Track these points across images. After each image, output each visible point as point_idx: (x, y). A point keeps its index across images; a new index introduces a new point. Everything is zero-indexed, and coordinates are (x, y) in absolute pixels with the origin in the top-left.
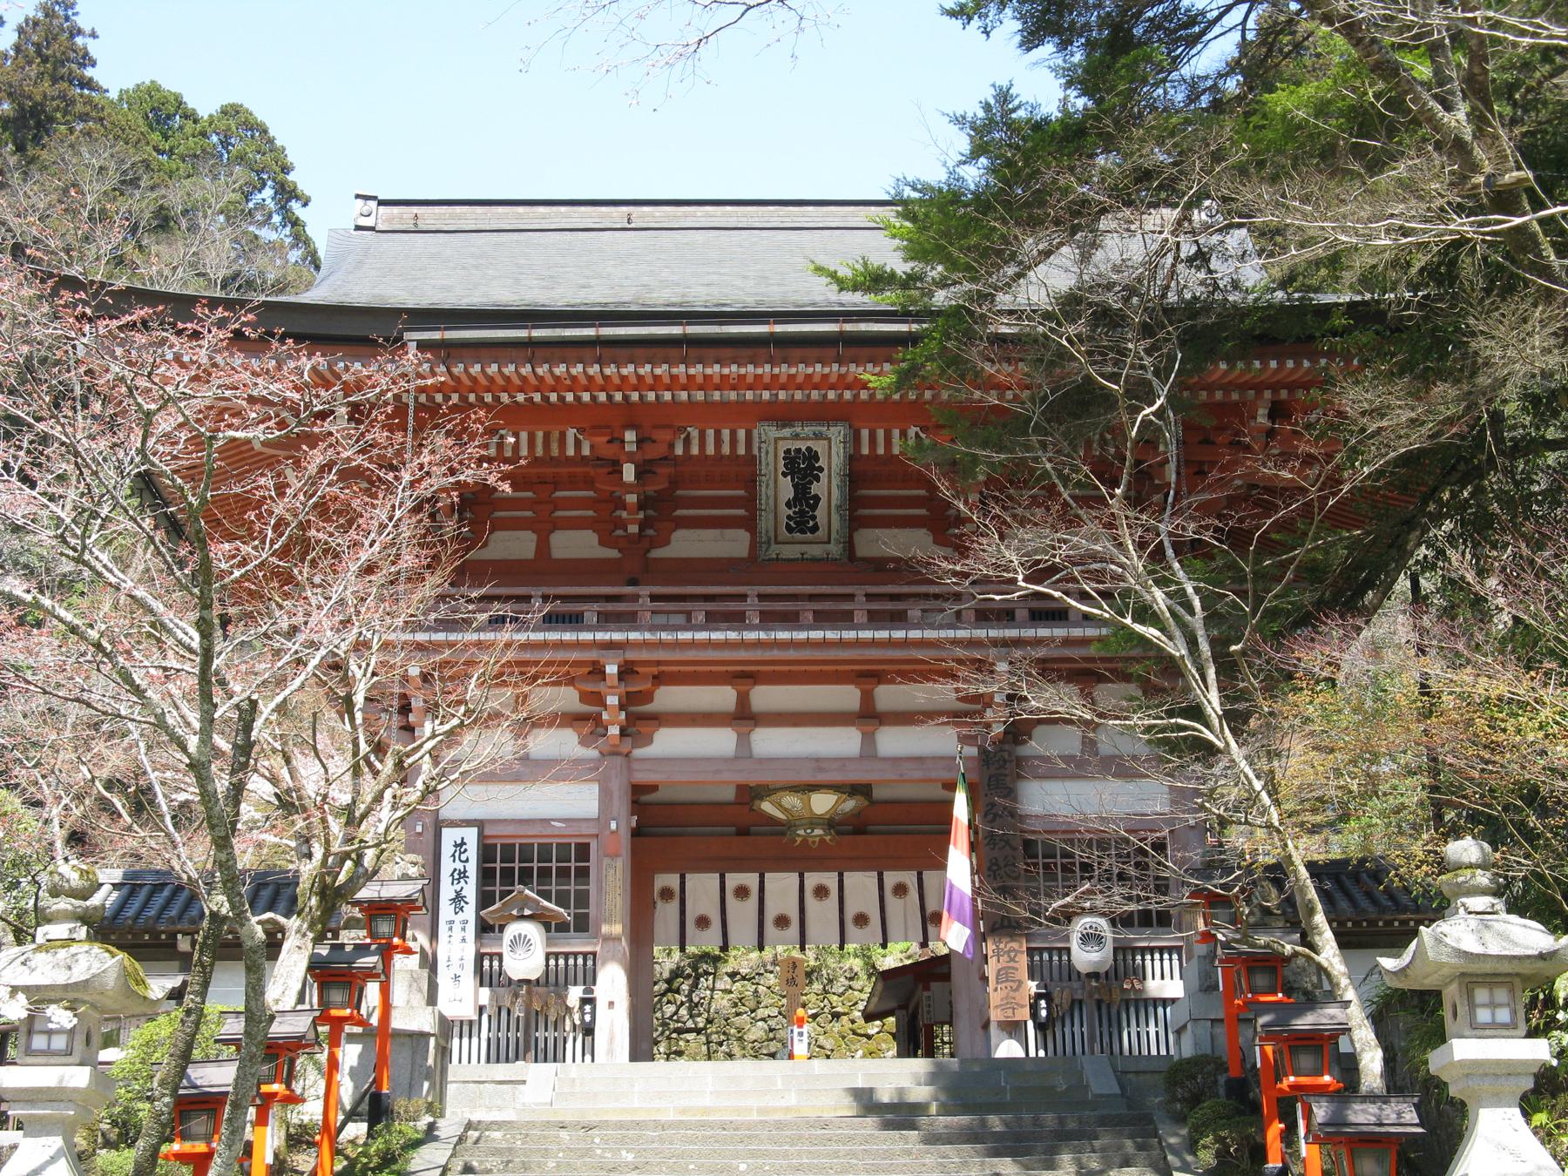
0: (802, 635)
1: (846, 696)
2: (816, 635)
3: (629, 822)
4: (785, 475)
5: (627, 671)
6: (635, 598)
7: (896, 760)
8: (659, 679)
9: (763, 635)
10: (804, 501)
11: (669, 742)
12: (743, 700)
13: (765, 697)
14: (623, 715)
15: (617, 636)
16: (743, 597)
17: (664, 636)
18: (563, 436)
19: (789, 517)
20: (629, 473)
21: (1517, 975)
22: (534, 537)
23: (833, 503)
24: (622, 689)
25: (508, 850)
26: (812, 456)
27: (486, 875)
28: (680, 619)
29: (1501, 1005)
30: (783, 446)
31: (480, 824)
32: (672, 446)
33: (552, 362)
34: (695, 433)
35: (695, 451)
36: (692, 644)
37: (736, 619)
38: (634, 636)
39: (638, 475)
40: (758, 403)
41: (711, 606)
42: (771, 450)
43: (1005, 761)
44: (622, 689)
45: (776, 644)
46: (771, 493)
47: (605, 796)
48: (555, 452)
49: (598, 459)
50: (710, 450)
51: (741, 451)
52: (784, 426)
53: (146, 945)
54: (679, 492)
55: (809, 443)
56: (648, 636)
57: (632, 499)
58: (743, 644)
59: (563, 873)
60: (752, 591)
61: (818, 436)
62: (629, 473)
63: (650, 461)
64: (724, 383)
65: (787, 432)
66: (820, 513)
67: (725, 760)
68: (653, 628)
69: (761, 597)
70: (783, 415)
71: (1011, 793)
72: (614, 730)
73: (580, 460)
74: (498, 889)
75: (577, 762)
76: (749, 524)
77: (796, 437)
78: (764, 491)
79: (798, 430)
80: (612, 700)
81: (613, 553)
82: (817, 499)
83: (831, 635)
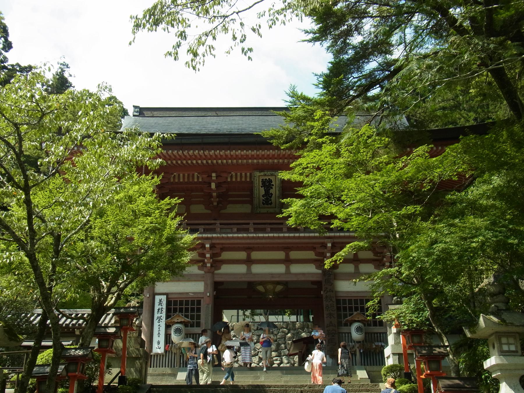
0: (267, 235)
1: (280, 255)
2: (271, 235)
3: (213, 293)
4: (262, 187)
5: (212, 246)
6: (215, 224)
7: (296, 274)
8: (223, 249)
9: (254, 235)
10: (268, 194)
11: (226, 269)
12: (249, 256)
13: (256, 255)
14: (211, 260)
15: (209, 235)
16: (248, 224)
17: (224, 235)
18: (193, 175)
19: (263, 200)
20: (213, 186)
21: (517, 333)
22: (185, 207)
23: (277, 195)
24: (211, 252)
25: (175, 302)
26: (270, 181)
27: (168, 310)
28: (229, 230)
29: (511, 344)
30: (261, 178)
31: (167, 294)
32: (227, 178)
33: (189, 150)
34: (233, 174)
35: (234, 180)
36: (233, 238)
37: (247, 231)
38: (214, 235)
39: (216, 187)
40: (253, 164)
41: (239, 226)
42: (258, 179)
43: (330, 275)
44: (211, 252)
45: (259, 238)
46: (258, 192)
47: (206, 284)
48: (191, 180)
49: (204, 182)
50: (239, 179)
51: (248, 180)
52: (261, 172)
53: (66, 333)
54: (229, 193)
55: (269, 177)
56: (219, 235)
57: (214, 194)
58: (248, 238)
59: (193, 310)
60: (251, 222)
61: (272, 175)
62: (213, 186)
63: (220, 183)
64: (242, 157)
65: (262, 174)
66: (273, 199)
67: (243, 274)
68: (220, 233)
69: (254, 224)
70: (261, 168)
71: (332, 284)
72: (209, 265)
73: (198, 183)
74: (172, 314)
75: (196, 275)
76: (251, 202)
77: (265, 175)
78: (256, 192)
79: (266, 173)
80: (208, 255)
81: (209, 212)
82: (272, 194)
83: (276, 235)
